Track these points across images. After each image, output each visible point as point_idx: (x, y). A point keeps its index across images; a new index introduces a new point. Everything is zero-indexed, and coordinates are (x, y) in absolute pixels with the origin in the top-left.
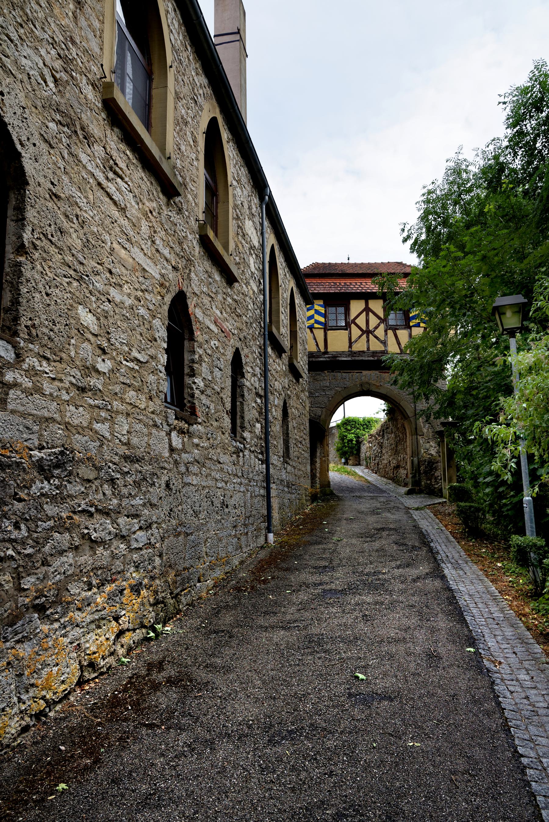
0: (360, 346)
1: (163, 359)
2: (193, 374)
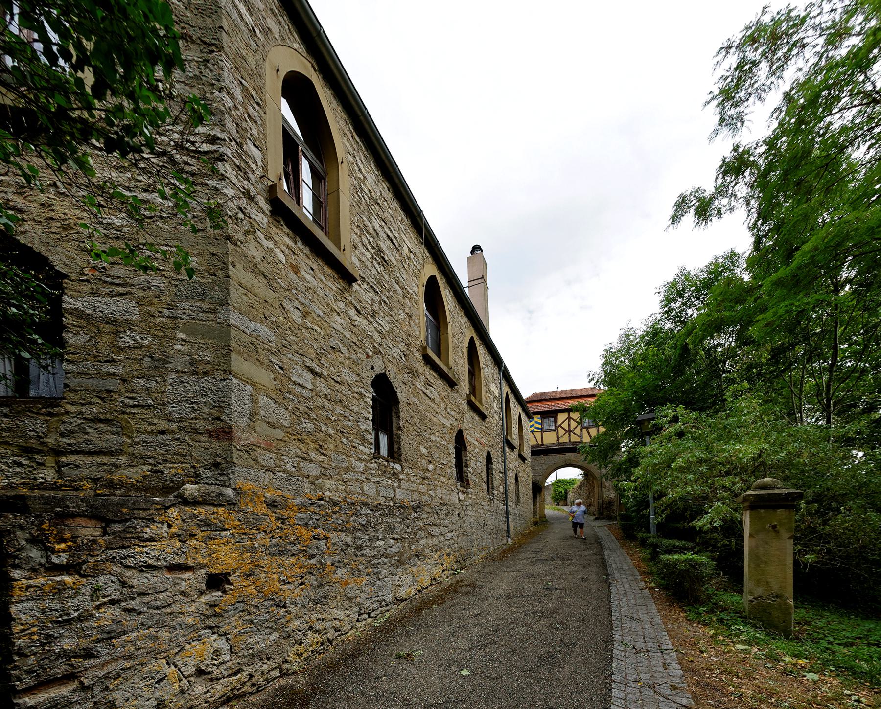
0: (565, 439)
1: (454, 461)
2: (467, 466)
